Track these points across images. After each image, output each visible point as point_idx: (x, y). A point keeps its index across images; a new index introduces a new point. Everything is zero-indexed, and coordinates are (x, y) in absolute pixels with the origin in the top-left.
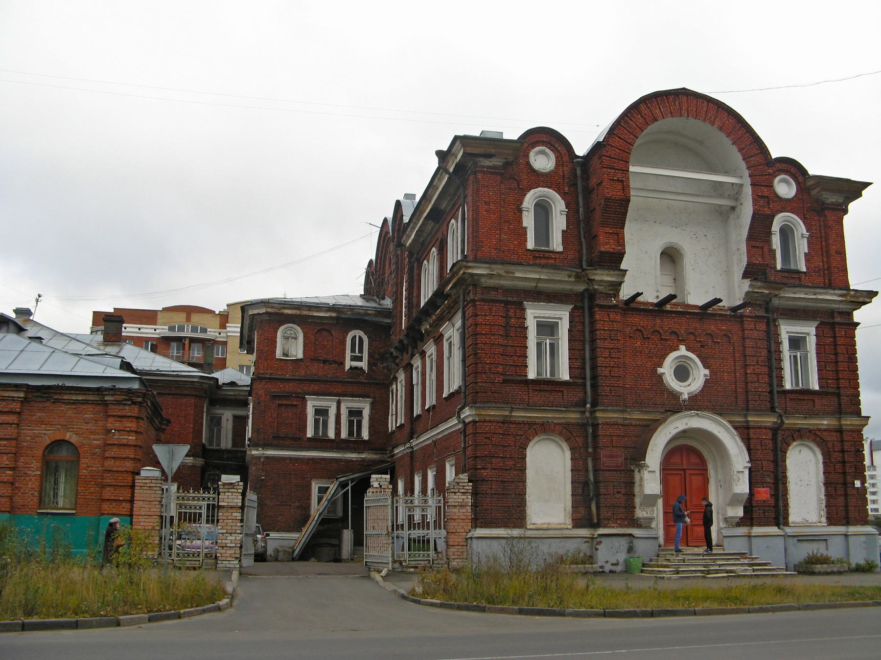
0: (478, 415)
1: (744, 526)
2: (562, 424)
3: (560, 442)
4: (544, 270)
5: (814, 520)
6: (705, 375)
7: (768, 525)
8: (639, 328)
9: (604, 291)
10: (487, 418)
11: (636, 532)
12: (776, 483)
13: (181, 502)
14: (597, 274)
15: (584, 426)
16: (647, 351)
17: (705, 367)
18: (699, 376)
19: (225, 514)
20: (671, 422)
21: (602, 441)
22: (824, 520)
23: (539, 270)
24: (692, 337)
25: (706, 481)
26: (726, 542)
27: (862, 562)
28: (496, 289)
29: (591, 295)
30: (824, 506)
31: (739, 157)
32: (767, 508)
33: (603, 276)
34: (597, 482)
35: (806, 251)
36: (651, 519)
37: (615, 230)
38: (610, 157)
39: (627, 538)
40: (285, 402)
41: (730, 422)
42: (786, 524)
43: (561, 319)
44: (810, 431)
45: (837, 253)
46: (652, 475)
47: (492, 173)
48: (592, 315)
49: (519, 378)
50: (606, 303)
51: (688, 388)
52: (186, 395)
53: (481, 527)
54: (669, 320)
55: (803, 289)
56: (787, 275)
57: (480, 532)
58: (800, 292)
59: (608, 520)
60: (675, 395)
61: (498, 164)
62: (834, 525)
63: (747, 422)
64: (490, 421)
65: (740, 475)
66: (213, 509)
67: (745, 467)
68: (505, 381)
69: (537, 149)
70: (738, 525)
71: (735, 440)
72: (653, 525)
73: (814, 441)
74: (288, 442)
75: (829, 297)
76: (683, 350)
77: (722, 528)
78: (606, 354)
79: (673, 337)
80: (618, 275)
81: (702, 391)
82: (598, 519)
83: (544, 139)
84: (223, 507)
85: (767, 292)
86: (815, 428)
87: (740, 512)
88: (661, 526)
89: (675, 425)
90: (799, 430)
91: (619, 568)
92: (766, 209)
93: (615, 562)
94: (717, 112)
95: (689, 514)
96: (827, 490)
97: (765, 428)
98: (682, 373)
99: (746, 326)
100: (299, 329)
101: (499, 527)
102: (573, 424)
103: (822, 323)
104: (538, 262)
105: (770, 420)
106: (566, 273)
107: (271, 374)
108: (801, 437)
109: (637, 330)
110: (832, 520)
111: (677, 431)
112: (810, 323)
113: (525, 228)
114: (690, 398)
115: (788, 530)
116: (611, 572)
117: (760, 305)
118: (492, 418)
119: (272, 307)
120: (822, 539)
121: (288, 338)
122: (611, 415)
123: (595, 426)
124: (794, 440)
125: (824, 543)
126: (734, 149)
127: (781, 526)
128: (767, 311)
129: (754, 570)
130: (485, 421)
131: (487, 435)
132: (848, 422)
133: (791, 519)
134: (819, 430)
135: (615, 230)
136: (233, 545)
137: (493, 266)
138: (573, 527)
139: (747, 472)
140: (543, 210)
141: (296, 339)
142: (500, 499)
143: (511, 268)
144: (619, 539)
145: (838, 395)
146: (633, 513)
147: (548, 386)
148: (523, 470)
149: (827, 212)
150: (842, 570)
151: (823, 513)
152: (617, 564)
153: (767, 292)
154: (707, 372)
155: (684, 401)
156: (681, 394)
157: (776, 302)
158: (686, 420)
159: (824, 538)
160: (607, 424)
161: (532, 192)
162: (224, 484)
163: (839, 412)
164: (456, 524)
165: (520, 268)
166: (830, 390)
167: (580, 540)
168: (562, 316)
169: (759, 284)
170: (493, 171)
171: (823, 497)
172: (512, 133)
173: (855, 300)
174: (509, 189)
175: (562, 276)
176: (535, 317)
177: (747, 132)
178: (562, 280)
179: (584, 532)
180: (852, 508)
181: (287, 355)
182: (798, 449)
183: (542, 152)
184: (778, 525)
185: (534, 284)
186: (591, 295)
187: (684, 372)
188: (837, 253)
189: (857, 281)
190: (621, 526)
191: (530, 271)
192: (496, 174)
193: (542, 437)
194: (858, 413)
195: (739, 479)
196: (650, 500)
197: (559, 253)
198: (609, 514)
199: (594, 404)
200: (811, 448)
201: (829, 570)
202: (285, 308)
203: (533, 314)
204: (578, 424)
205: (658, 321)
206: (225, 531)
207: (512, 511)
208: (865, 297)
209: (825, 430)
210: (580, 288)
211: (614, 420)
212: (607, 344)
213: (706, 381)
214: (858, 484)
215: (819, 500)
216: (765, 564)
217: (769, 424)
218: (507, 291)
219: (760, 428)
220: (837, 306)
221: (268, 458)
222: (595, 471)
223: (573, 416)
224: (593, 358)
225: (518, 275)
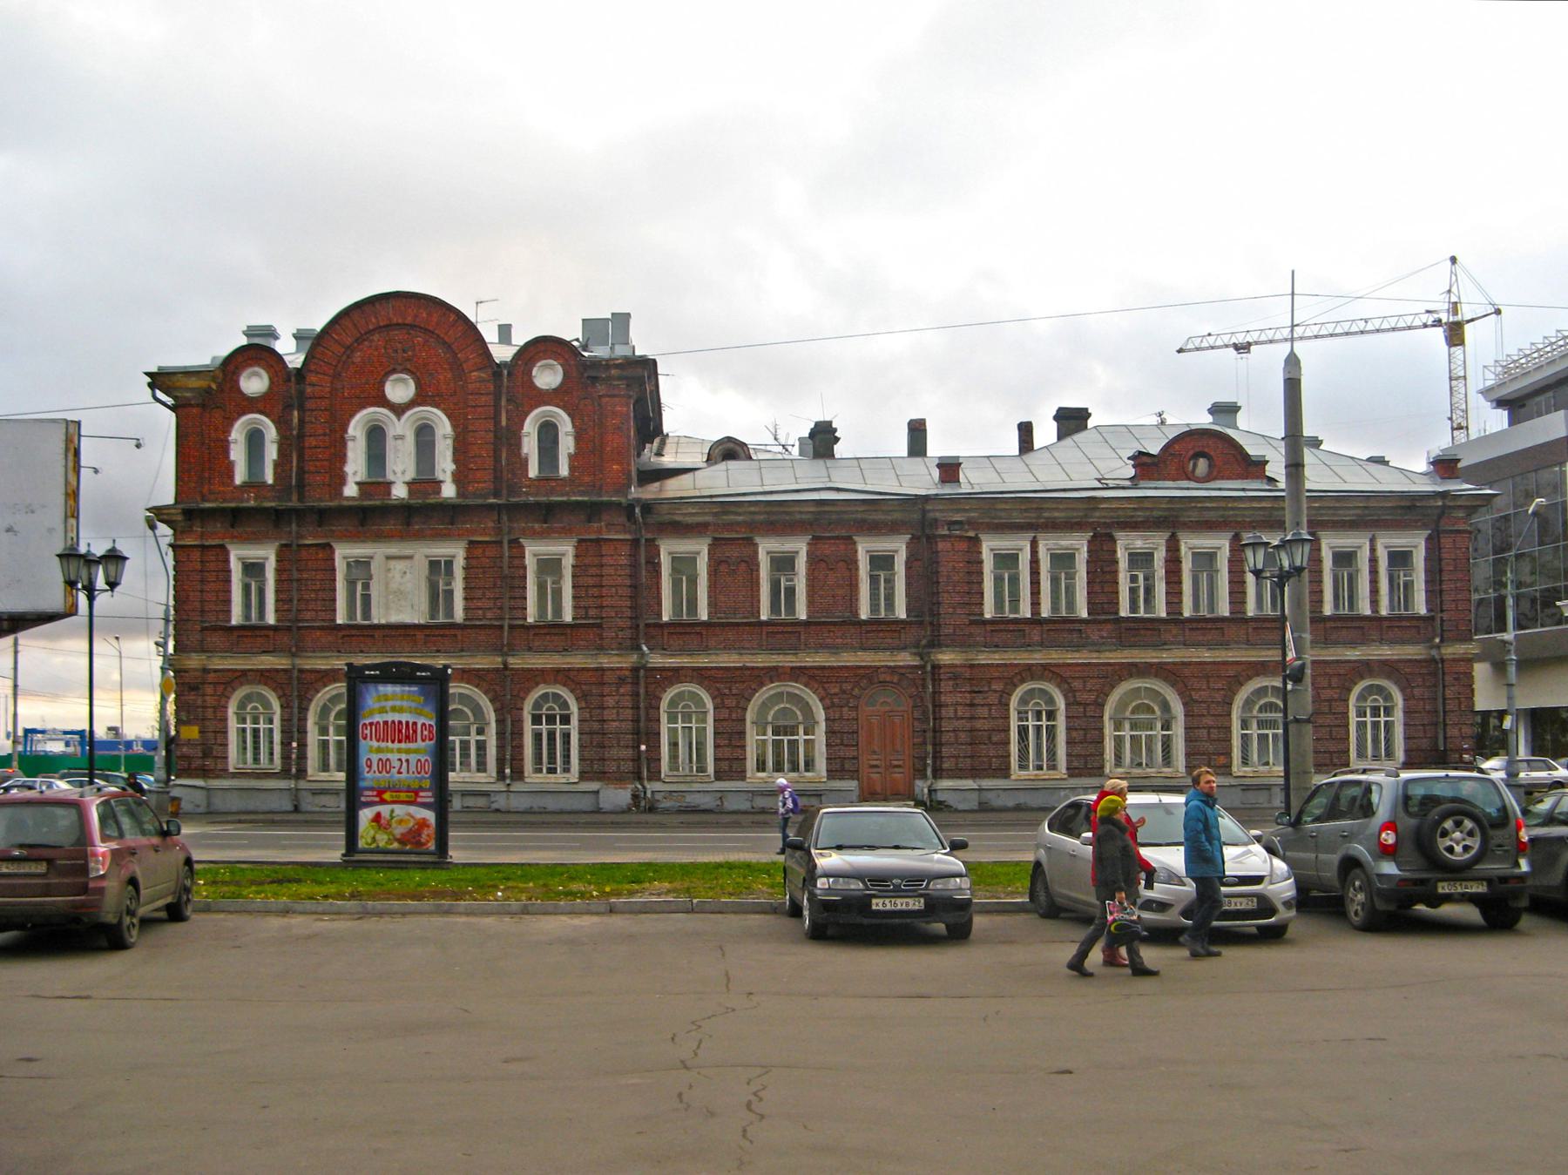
24: (823, 565)
68: (204, 629)
115: (302, 784)
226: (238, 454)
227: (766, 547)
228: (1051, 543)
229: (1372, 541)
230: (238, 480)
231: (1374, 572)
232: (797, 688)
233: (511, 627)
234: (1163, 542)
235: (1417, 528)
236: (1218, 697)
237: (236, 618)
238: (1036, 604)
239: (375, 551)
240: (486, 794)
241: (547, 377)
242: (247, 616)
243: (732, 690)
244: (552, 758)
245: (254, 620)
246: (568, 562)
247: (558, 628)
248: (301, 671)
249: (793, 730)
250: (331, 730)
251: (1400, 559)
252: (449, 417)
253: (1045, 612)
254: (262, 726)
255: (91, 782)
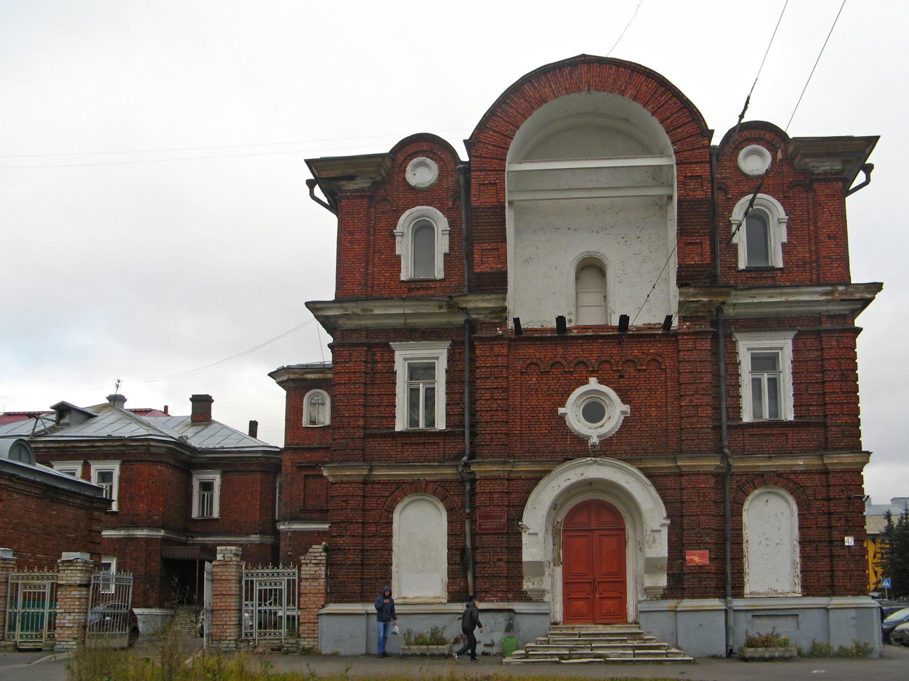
0: (333, 476)
1: (672, 598)
2: (437, 481)
3: (431, 500)
4: (406, 303)
5: (787, 590)
6: (623, 412)
7: (705, 597)
8: (535, 361)
9: (487, 320)
10: (345, 479)
11: (519, 607)
12: (721, 544)
13: (25, 582)
14: (469, 301)
15: (462, 482)
16: (545, 388)
17: (624, 401)
18: (616, 411)
19: (64, 593)
20: (562, 473)
21: (480, 500)
22: (798, 589)
23: (401, 303)
24: (607, 366)
25: (623, 544)
26: (642, 619)
27: (849, 645)
28: (356, 330)
29: (472, 326)
30: (798, 571)
31: (661, 130)
32: (704, 576)
33: (481, 303)
34: (474, 549)
35: (785, 240)
36: (543, 592)
37: (494, 245)
38: (481, 157)
39: (506, 615)
40: (311, 473)
41: (640, 469)
42: (738, 592)
43: (437, 358)
44: (779, 475)
45: (829, 238)
46: (533, 538)
47: (358, 197)
48: (472, 348)
49: (385, 431)
50: (489, 334)
51: (600, 429)
52: (253, 471)
53: (689, 598)
54: (569, 351)
55: (762, 291)
56: (754, 275)
57: (333, 608)
58: (762, 295)
59: (487, 592)
60: (582, 440)
61: (365, 185)
62: (813, 596)
63: (825, 465)
64: (347, 482)
65: (657, 535)
66: (56, 587)
67: (663, 525)
68: (366, 436)
69: (415, 161)
70: (664, 597)
71: (650, 492)
72: (547, 598)
73: (785, 487)
74: (315, 515)
75: (807, 298)
76: (593, 383)
77: (640, 602)
78: (488, 396)
79: (581, 367)
80: (498, 299)
81: (619, 432)
82: (475, 593)
83: (425, 148)
84: (61, 585)
85: (705, 299)
86: (788, 470)
87: (662, 581)
88: (559, 598)
89: (566, 475)
90: (762, 475)
91: (494, 650)
92: (698, 193)
93: (489, 642)
94: (630, 78)
95: (595, 587)
96: (802, 551)
97: (705, 474)
98: (594, 412)
99: (681, 347)
100: (325, 394)
101: (356, 602)
102: (451, 481)
103: (800, 333)
104: (412, 294)
105: (711, 463)
106: (436, 303)
107: (298, 444)
108: (765, 483)
109: (532, 363)
110: (808, 589)
111: (568, 483)
112: (784, 333)
113: (399, 257)
114: (601, 442)
115: (738, 603)
116: (484, 654)
117: (704, 318)
118: (350, 479)
119: (295, 373)
120: (791, 614)
121: (315, 404)
122: (488, 468)
123: (473, 481)
124: (756, 488)
125: (794, 619)
126: (655, 121)
127: (729, 598)
128: (714, 324)
129: (635, 655)
130: (342, 483)
131: (345, 499)
132: (839, 460)
133: (747, 590)
134: (795, 473)
135: (494, 245)
136: (71, 625)
137: (346, 305)
138: (449, 601)
139: (665, 531)
140: (423, 229)
141: (323, 404)
142: (363, 572)
143: (368, 305)
144: (495, 615)
145: (825, 426)
146: (520, 584)
147: (419, 439)
148: (389, 536)
149: (816, 185)
150: (787, 655)
151: (798, 581)
152: (491, 645)
153: (705, 299)
154: (627, 408)
155: (594, 446)
156: (589, 437)
157: (729, 312)
158: (580, 470)
159: (795, 612)
160: (486, 479)
161: (407, 213)
162: (63, 562)
163: (825, 448)
164: (307, 599)
165: (377, 303)
166: (813, 419)
167: (452, 616)
168: (439, 355)
169: (692, 290)
170: (360, 194)
171: (798, 560)
172: (385, 147)
173: (848, 297)
174: (382, 213)
175: (430, 308)
176: (405, 359)
177: (674, 96)
178: (429, 313)
179: (460, 607)
180: (840, 573)
181: (314, 423)
182: (763, 499)
183: (423, 164)
184: (723, 596)
185: (402, 321)
186: (472, 326)
187: (594, 410)
188: (829, 238)
189: (859, 275)
190: (502, 600)
191: (391, 306)
192: (363, 197)
193: (414, 498)
194: (856, 447)
195: (654, 541)
196: (538, 568)
197: (440, 280)
198: (487, 586)
199: (472, 456)
200: (778, 494)
201: (767, 655)
202: (307, 373)
203: (403, 356)
204: (457, 481)
205: (560, 350)
206: (63, 611)
207: (726, 577)
208: (863, 292)
209: (803, 473)
210: (460, 319)
211: (495, 474)
212: (489, 384)
213: (626, 420)
214: (849, 541)
215: (794, 563)
216: (658, 647)
217: (712, 469)
218: (367, 330)
219: (698, 474)
220: (824, 308)
221: (294, 532)
222: (473, 535)
223: (448, 472)
224: (473, 402)
225: (376, 312)
226: (404, 247)
228: (409, 353)
230: (742, 265)
233: (729, 427)
234: (445, 351)
235: (788, 330)
237: (401, 425)
241: (755, 162)
242: (414, 422)
247: (776, 425)
252: (783, 205)
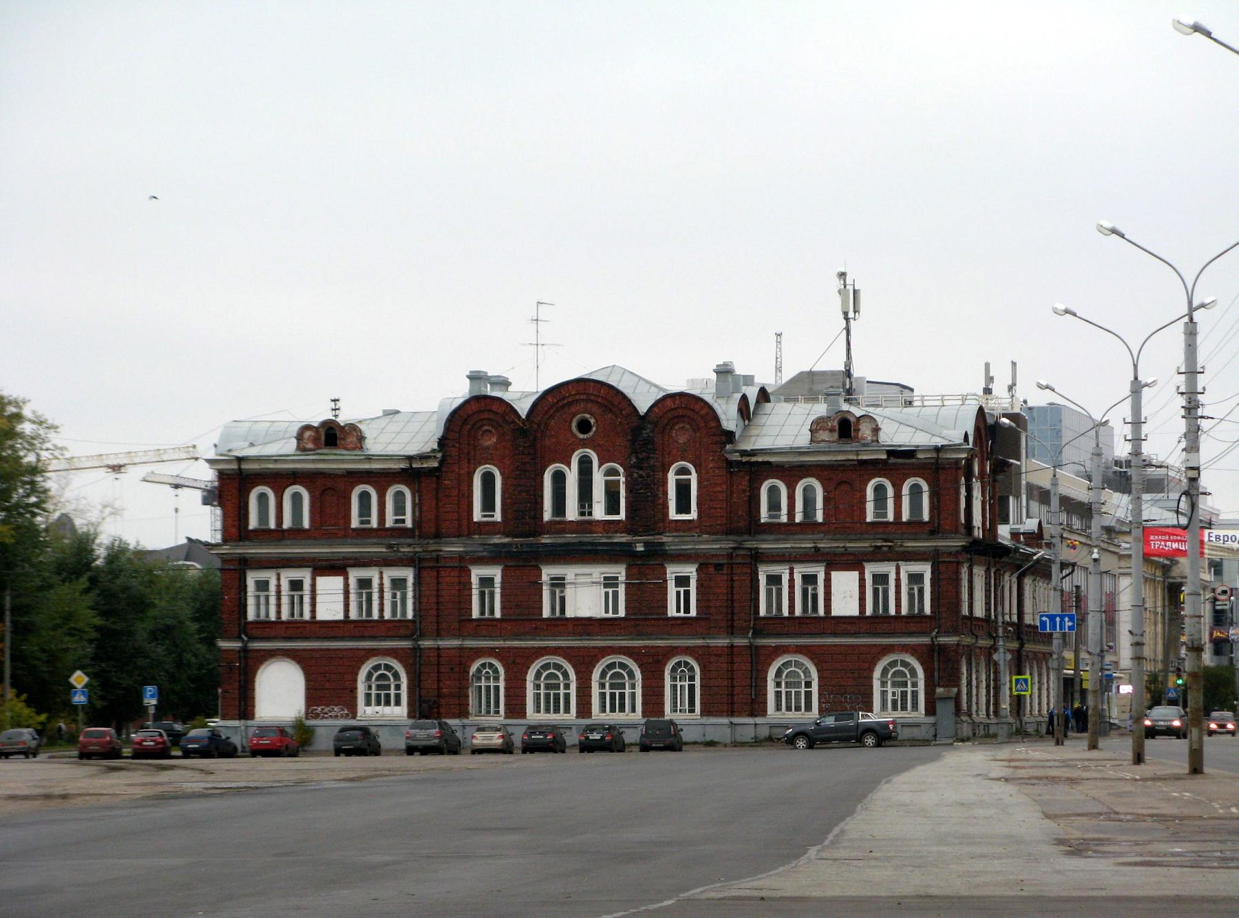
227: (477, 573)
229: (381, 573)
231: (898, 587)
232: (383, 661)
236: (866, 665)
238: (381, 610)
239: (570, 572)
240: (917, 725)
243: (517, 665)
244: (488, 705)
245: (296, 617)
246: (498, 580)
248: (757, 647)
249: (798, 685)
250: (607, 685)
251: (398, 584)
253: (353, 615)
254: (492, 684)
255: (1131, 718)
